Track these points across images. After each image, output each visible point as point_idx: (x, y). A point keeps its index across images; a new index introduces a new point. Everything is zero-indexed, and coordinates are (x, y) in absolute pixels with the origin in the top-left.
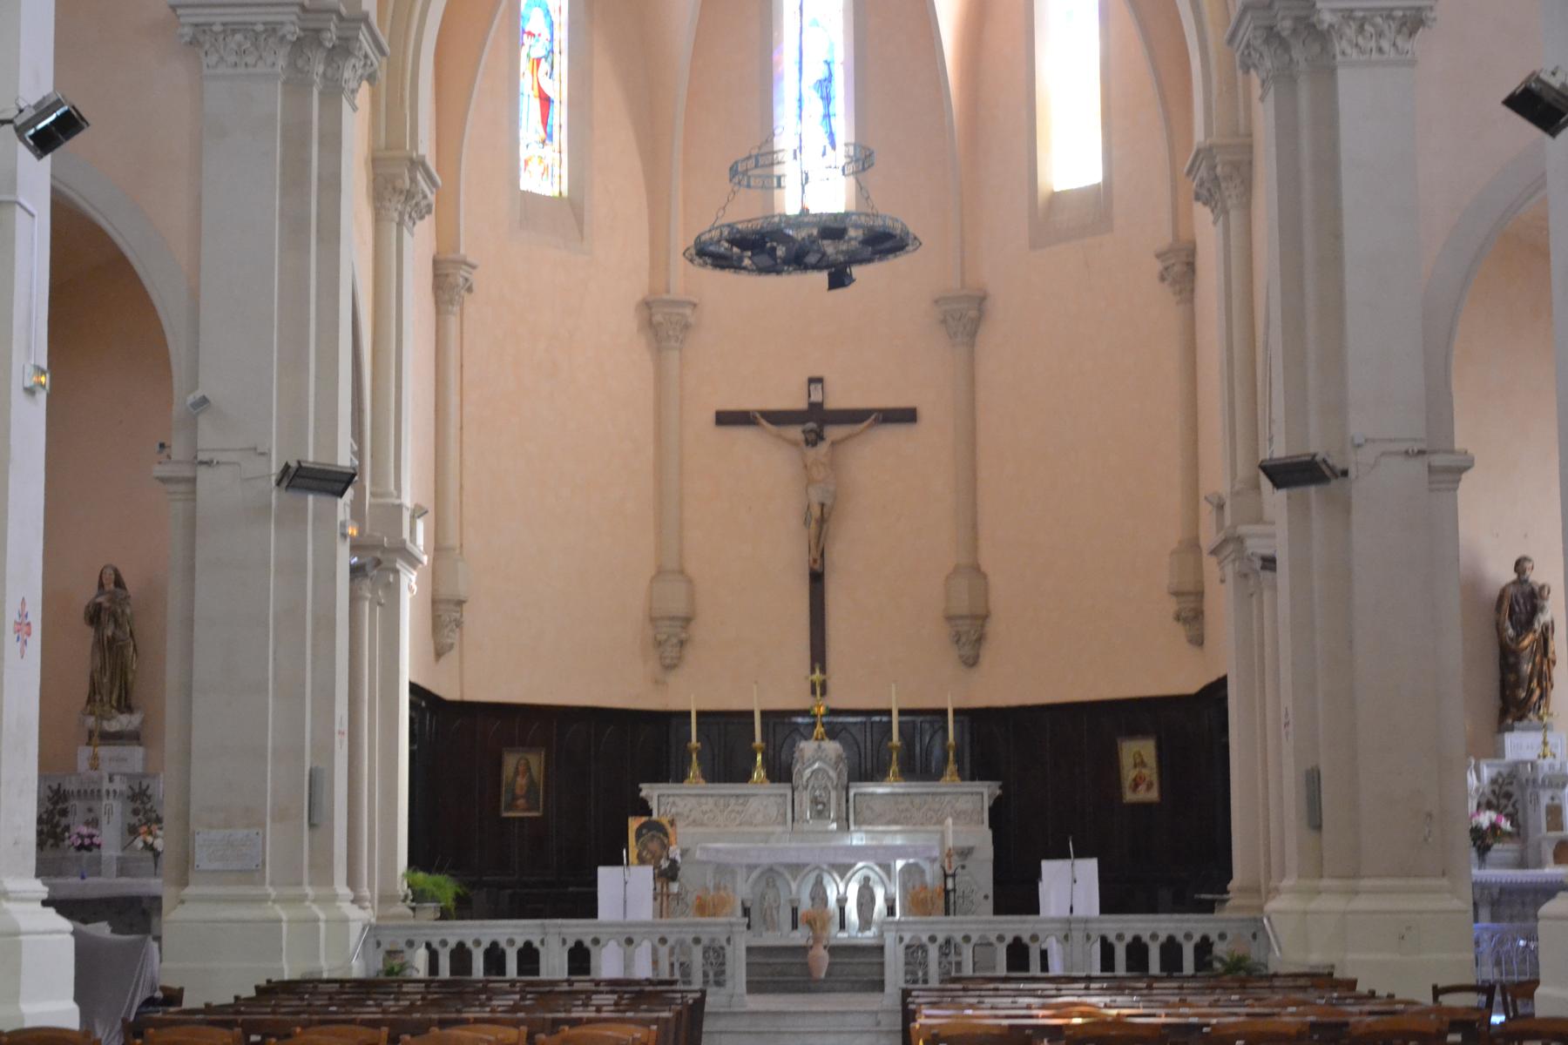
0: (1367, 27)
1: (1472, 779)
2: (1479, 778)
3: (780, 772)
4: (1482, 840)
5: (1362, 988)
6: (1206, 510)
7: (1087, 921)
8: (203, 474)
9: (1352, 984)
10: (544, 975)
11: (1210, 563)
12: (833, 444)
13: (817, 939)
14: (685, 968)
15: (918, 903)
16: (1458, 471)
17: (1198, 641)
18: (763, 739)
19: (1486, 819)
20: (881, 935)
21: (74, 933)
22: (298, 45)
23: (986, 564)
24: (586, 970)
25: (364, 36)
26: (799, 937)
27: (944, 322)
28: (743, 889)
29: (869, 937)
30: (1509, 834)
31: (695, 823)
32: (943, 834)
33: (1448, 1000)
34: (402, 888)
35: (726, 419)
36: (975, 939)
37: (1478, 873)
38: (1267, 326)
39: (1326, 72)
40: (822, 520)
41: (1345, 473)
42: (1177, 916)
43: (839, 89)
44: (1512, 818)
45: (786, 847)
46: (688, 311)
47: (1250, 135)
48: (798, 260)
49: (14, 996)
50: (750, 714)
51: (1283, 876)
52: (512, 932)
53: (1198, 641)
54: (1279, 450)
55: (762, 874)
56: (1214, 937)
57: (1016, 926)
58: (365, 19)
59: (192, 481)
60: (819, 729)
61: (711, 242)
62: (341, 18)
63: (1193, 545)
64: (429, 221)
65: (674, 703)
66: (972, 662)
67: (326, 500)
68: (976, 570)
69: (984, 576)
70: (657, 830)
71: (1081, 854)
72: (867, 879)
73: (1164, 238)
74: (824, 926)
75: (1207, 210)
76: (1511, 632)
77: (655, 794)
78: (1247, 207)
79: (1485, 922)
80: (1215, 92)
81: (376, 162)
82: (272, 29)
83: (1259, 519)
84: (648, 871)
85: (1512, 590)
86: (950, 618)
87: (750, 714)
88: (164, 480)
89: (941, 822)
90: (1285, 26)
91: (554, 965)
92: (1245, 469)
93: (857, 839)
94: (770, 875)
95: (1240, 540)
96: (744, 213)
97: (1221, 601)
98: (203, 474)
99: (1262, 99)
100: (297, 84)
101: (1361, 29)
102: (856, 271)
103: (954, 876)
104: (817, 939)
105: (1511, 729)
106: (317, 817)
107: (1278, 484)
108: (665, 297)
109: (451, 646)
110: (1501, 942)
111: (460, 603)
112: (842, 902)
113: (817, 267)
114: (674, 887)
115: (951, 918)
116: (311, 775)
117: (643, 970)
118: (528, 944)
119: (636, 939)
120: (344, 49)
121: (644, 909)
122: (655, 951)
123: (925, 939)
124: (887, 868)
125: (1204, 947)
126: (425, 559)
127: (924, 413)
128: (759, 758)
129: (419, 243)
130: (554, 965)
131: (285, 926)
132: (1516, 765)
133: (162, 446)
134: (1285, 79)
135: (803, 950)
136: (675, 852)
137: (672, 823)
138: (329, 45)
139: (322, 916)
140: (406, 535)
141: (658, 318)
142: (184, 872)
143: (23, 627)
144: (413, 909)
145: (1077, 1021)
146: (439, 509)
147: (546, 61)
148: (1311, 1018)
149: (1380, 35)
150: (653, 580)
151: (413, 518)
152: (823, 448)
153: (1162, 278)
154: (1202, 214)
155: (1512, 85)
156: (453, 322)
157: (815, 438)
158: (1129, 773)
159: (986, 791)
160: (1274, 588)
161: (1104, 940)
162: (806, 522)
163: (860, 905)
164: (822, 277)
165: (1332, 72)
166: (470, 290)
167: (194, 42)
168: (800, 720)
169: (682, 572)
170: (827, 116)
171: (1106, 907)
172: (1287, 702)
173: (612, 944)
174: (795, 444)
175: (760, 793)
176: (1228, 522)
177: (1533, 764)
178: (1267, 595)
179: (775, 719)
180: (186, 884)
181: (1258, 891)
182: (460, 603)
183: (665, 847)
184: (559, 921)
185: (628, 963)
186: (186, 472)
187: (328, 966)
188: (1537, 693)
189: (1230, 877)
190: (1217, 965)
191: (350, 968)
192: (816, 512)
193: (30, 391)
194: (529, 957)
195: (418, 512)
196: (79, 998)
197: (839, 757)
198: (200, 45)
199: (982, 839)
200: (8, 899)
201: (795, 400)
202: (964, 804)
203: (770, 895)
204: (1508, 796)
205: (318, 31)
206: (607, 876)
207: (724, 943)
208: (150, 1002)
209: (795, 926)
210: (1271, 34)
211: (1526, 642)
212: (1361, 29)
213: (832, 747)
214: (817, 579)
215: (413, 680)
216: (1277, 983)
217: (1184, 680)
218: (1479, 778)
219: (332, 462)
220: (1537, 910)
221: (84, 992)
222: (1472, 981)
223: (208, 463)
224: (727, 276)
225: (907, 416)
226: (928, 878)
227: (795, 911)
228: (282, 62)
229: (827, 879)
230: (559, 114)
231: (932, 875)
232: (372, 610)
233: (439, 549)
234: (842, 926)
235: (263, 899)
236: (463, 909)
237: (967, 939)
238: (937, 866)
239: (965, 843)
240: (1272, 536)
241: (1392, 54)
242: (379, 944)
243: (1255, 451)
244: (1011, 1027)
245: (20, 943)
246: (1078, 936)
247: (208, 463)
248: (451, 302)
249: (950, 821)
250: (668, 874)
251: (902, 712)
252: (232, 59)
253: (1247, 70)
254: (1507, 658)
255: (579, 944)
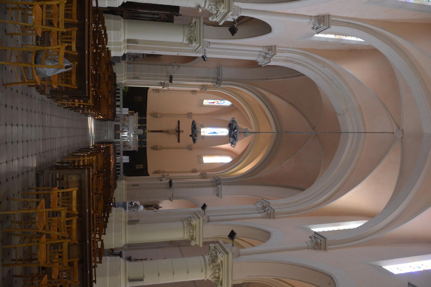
0: (217, 191)
1: (138, 202)
2: (138, 203)
3: (139, 128)
4: (131, 203)
5: (115, 190)
6: (167, 174)
7: (122, 161)
8: (172, 67)
9: (115, 189)
10: (117, 102)
11: (161, 174)
12: (176, 133)
13: (120, 131)
14: (117, 118)
15: (124, 143)
16: (171, 200)
17: (154, 173)
18: (143, 126)
19: (134, 204)
20: (121, 139)
21: (121, 56)
22: (218, 79)
23: (162, 150)
24: (117, 101)
25: (218, 85)
26: (121, 130)
27: (189, 145)
28: (126, 123)
29: (121, 137)
30: (132, 206)
31: (134, 118)
32: (132, 145)
33: (113, 199)
34: (126, 86)
35: (179, 122)
36: (120, 149)
37: (128, 203)
38: (186, 180)
39: (213, 186)
40: (167, 132)
41: (171, 188)
42: (123, 171)
43: (214, 134)
44: (134, 206)
45: (131, 128)
46: (191, 118)
47: (207, 178)
48: (193, 132)
49: (114, 51)
50: (146, 124)
51: (127, 182)
52: (121, 99)
53: (154, 173)
54: (173, 181)
55: (128, 126)
56: (120, 175)
57: (122, 153)
58: (220, 85)
59: (171, 66)
60: (144, 132)
61: (195, 122)
62: (220, 83)
63: (164, 172)
64: (200, 90)
65: (147, 116)
66: (152, 148)
67: (169, 80)
68: (162, 149)
69: (161, 150)
70: (132, 114)
71: (130, 161)
72: (127, 137)
73: (197, 169)
74: (122, 132)
75: (200, 174)
76: (154, 206)
77: (137, 114)
78: (200, 178)
79: (122, 204)
80: (212, 175)
81: (206, 85)
82: (219, 76)
83: (166, 179)
84: (128, 114)
85: (158, 206)
86: (156, 146)
87: (146, 124)
88: (171, 62)
89: (134, 145)
90: (218, 182)
91: (118, 103)
92: (172, 178)
93: (132, 136)
94: (128, 126)
95: (164, 177)
96: (198, 126)
97: (158, 175)
98: (172, 67)
99: (210, 180)
100: (213, 78)
101: (217, 190)
102: (192, 138)
103: (127, 146)
104: (120, 131)
105: (143, 206)
106: (134, 78)
107: (169, 181)
108: (192, 115)
109: (154, 91)
110: (120, 205)
111: (158, 92)
112: (125, 134)
113: (192, 134)
114: (126, 116)
115: (123, 146)
116: (139, 77)
117: (117, 113)
118: (120, 101)
119: (120, 112)
120: (217, 83)
121: (124, 113)
122: (119, 114)
123: (120, 144)
124: (128, 139)
125: (119, 174)
126: (163, 89)
127: (179, 143)
128: (141, 125)
129: (198, 89)
130: (118, 103)
131: (122, 74)
132: (139, 207)
133: (175, 62)
134: (212, 182)
135: (119, 130)
136: (130, 116)
137: (133, 116)
138: (217, 82)
139: (123, 78)
140: (166, 87)
141: (190, 114)
142: (128, 63)
143: (153, 52)
144: (124, 87)
145: (111, 161)
146: (168, 90)
147: (68, 210)
148: (111, 185)
149: (216, 192)
150: (161, 113)
151: (168, 88)
152: (175, 132)
153: (193, 169)
154: (199, 173)
155: (206, 204)
156: (190, 92)
157: (176, 131)
158: (139, 165)
159: (137, 150)
160: (159, 181)
161: (120, 163)
162: (167, 130)
163: (124, 136)
164: (191, 134)
165: (213, 187)
166: (193, 94)
167: (218, 67)
168: (145, 129)
169: (162, 116)
170: (212, 133)
171: (124, 163)
172: (146, 182)
173: (120, 110)
174: (176, 129)
175: (137, 125)
176: (166, 176)
177: (140, 209)
178: (158, 180)
179: (146, 127)
180: (127, 63)
181: (126, 180)
182: (158, 92)
183: (131, 115)
184: (122, 104)
185: (118, 111)
186: (172, 65)
187: (118, 79)
188: (147, 209)
189: (127, 176)
190: (117, 175)
191: (117, 81)
192: (169, 131)
193: (178, 54)
194: (119, 101)
195: (168, 88)
196: (114, 57)
197: (141, 134)
198: (218, 68)
199: (132, 149)
200: (125, 50)
201: (180, 129)
202: (135, 147)
203: (125, 126)
204: (136, 206)
205: (219, 81)
206: (127, 109)
207: (120, 122)
208: (114, 63)
209: (122, 129)
210: (217, 181)
211: (153, 208)
212: (217, 190)
213: (142, 133)
214: (161, 131)
215: (149, 88)
216: (115, 182)
217: (150, 171)
218: (138, 203)
219: (173, 80)
220: (123, 208)
221: (115, 57)
222: (115, 202)
223: (173, 67)
224: (191, 124)
225: (179, 141)
226: (127, 144)
227: (124, 129)
228: (216, 77)
229: (127, 132)
230: (212, 104)
231: (128, 144)
232: (157, 83)
233: (164, 90)
234: (122, 134)
235: (125, 72)
236: (124, 92)
237: (120, 148)
238: (129, 145)
239: (131, 148)
240: (165, 181)
241: (214, 193)
242: (120, 84)
243: (173, 179)
244: (111, 155)
245: (119, 20)
246: (120, 160)
247: (173, 67)
248: (192, 92)
249: (133, 146)
250: (128, 115)
251: (146, 141)
252: (216, 71)
253: (213, 178)
254: (151, 206)
255: (120, 106)
